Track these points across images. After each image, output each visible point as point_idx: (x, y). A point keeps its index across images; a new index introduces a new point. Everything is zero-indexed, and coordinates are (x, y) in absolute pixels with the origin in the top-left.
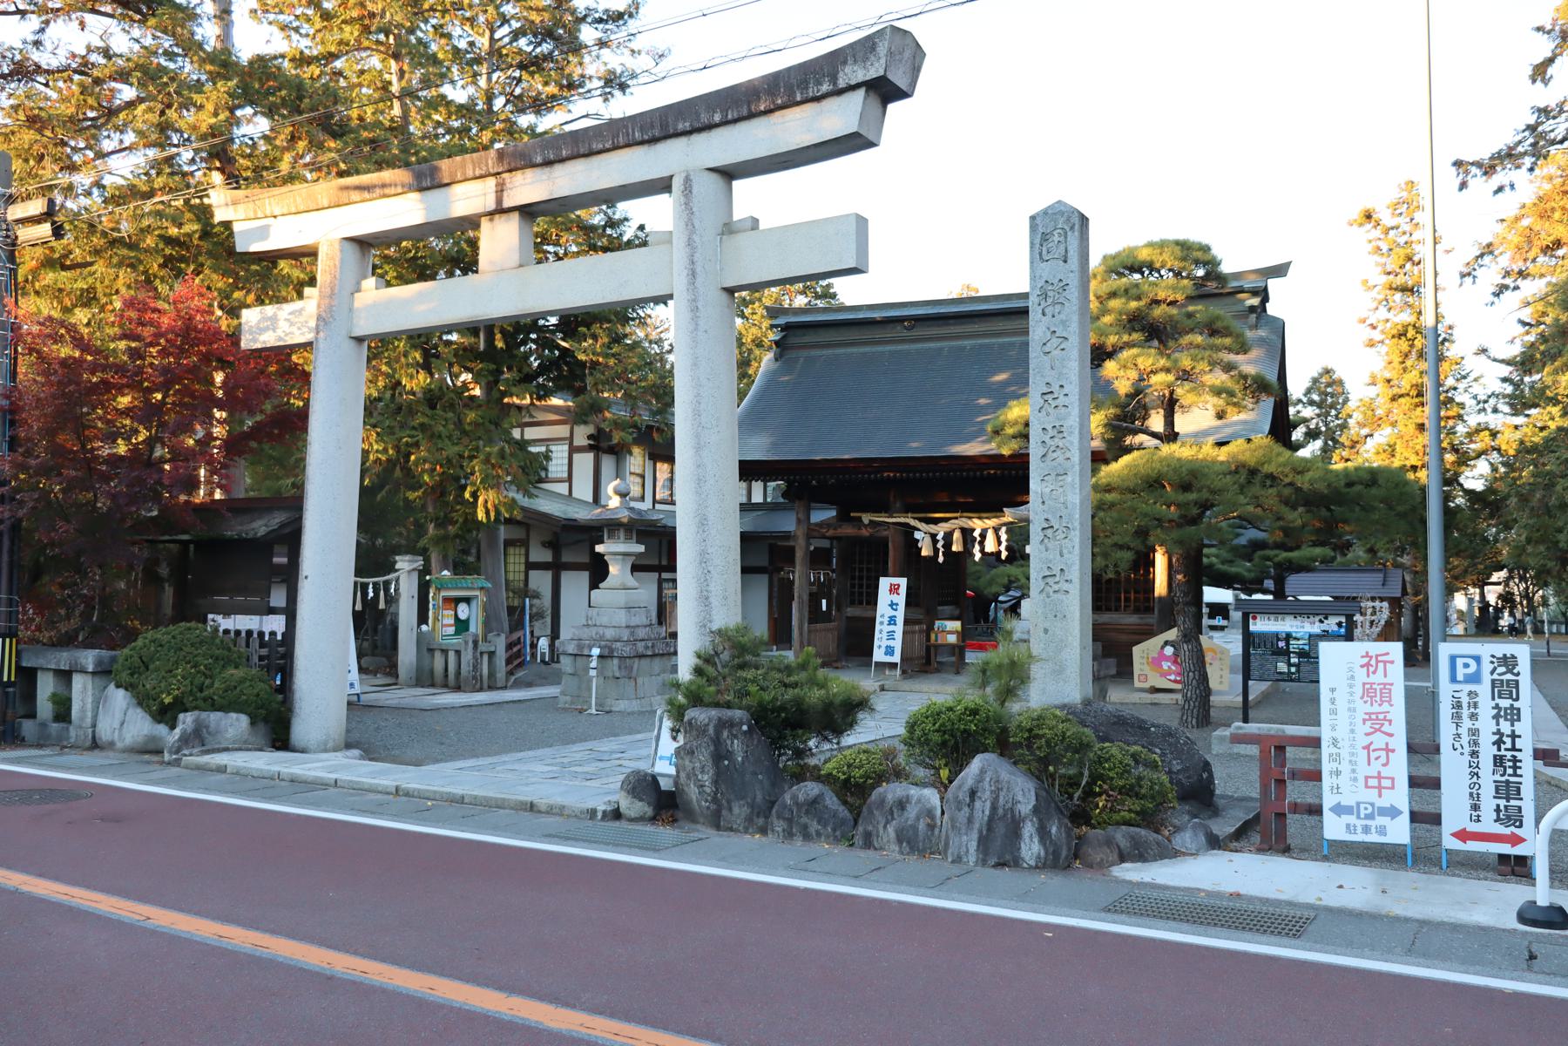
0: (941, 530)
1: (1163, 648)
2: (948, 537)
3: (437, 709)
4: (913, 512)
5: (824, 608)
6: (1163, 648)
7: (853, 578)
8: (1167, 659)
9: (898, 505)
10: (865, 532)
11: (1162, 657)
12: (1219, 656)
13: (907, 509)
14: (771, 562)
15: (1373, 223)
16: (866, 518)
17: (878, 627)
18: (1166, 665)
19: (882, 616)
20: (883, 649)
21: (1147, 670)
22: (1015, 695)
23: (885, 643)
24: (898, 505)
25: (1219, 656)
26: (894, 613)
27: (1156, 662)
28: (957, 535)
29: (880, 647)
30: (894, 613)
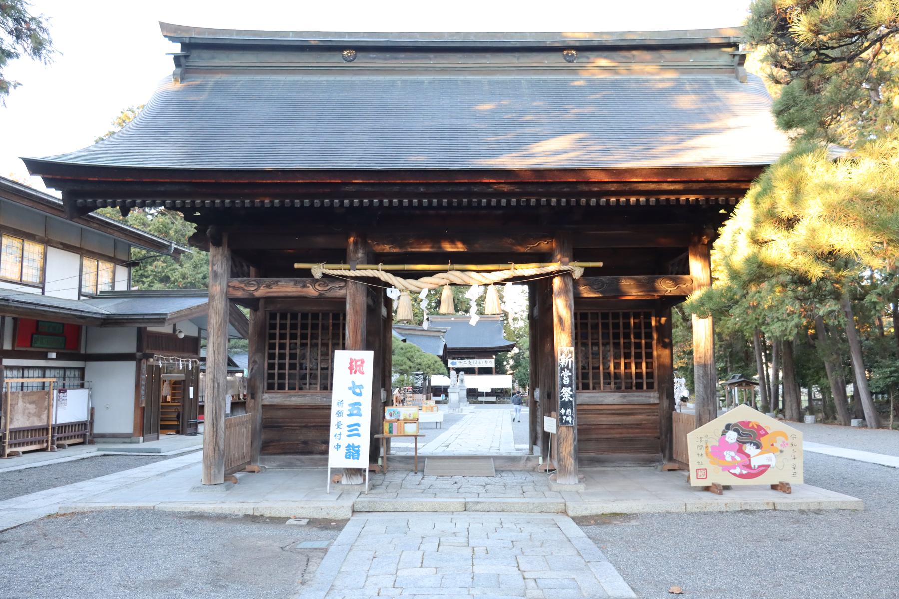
0: (425, 284)
1: (724, 433)
2: (436, 292)
3: (265, 348)
4: (385, 263)
5: (191, 396)
6: (724, 433)
7: (271, 357)
8: (729, 447)
9: (360, 255)
10: (312, 291)
11: (724, 445)
12: (790, 441)
13: (375, 259)
14: (139, 349)
16: (318, 270)
17: (334, 420)
18: (729, 455)
19: (340, 403)
20: (343, 451)
21: (706, 462)
23: (345, 441)
24: (360, 255)
25: (790, 441)
26: (357, 399)
27: (717, 452)
28: (447, 292)
29: (338, 447)
30: (357, 399)
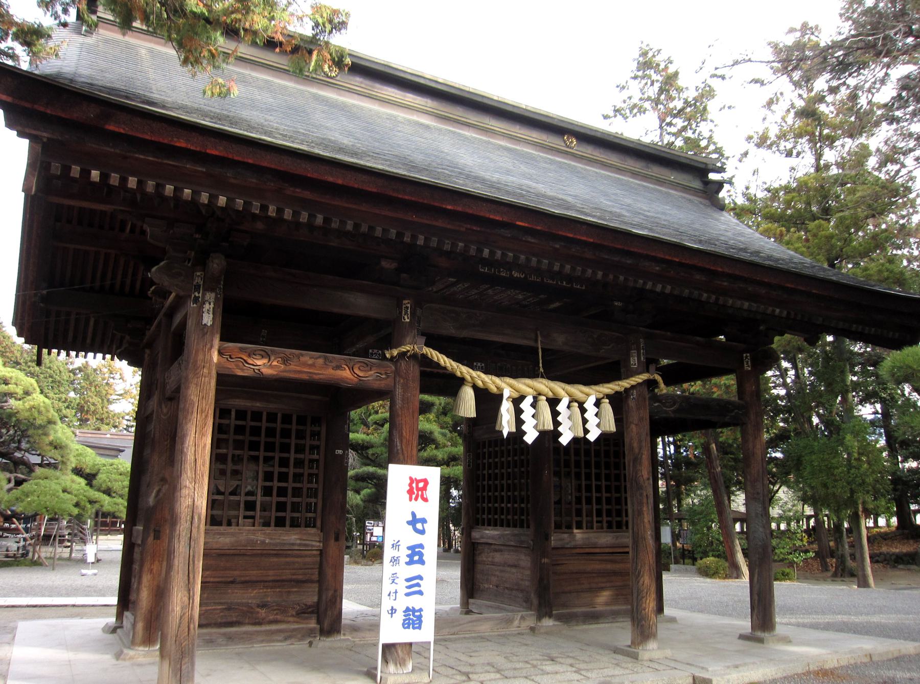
15: (846, 87)
19: (395, 546)
20: (399, 617)
22: (893, 678)
26: (416, 539)
